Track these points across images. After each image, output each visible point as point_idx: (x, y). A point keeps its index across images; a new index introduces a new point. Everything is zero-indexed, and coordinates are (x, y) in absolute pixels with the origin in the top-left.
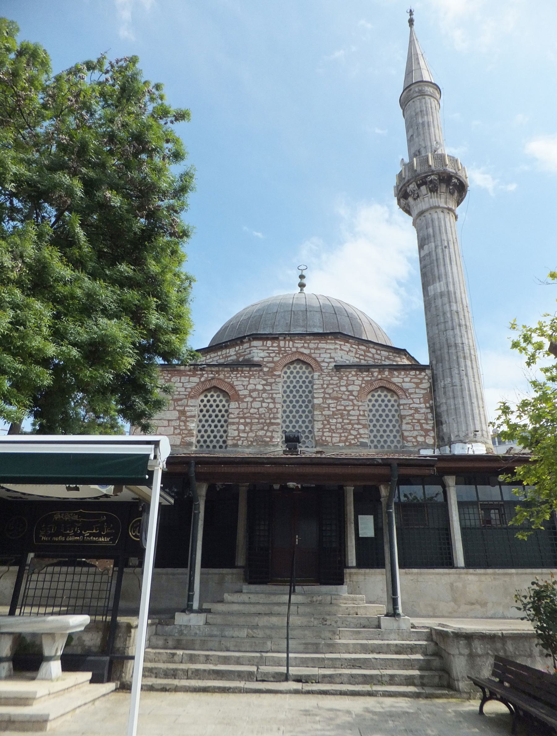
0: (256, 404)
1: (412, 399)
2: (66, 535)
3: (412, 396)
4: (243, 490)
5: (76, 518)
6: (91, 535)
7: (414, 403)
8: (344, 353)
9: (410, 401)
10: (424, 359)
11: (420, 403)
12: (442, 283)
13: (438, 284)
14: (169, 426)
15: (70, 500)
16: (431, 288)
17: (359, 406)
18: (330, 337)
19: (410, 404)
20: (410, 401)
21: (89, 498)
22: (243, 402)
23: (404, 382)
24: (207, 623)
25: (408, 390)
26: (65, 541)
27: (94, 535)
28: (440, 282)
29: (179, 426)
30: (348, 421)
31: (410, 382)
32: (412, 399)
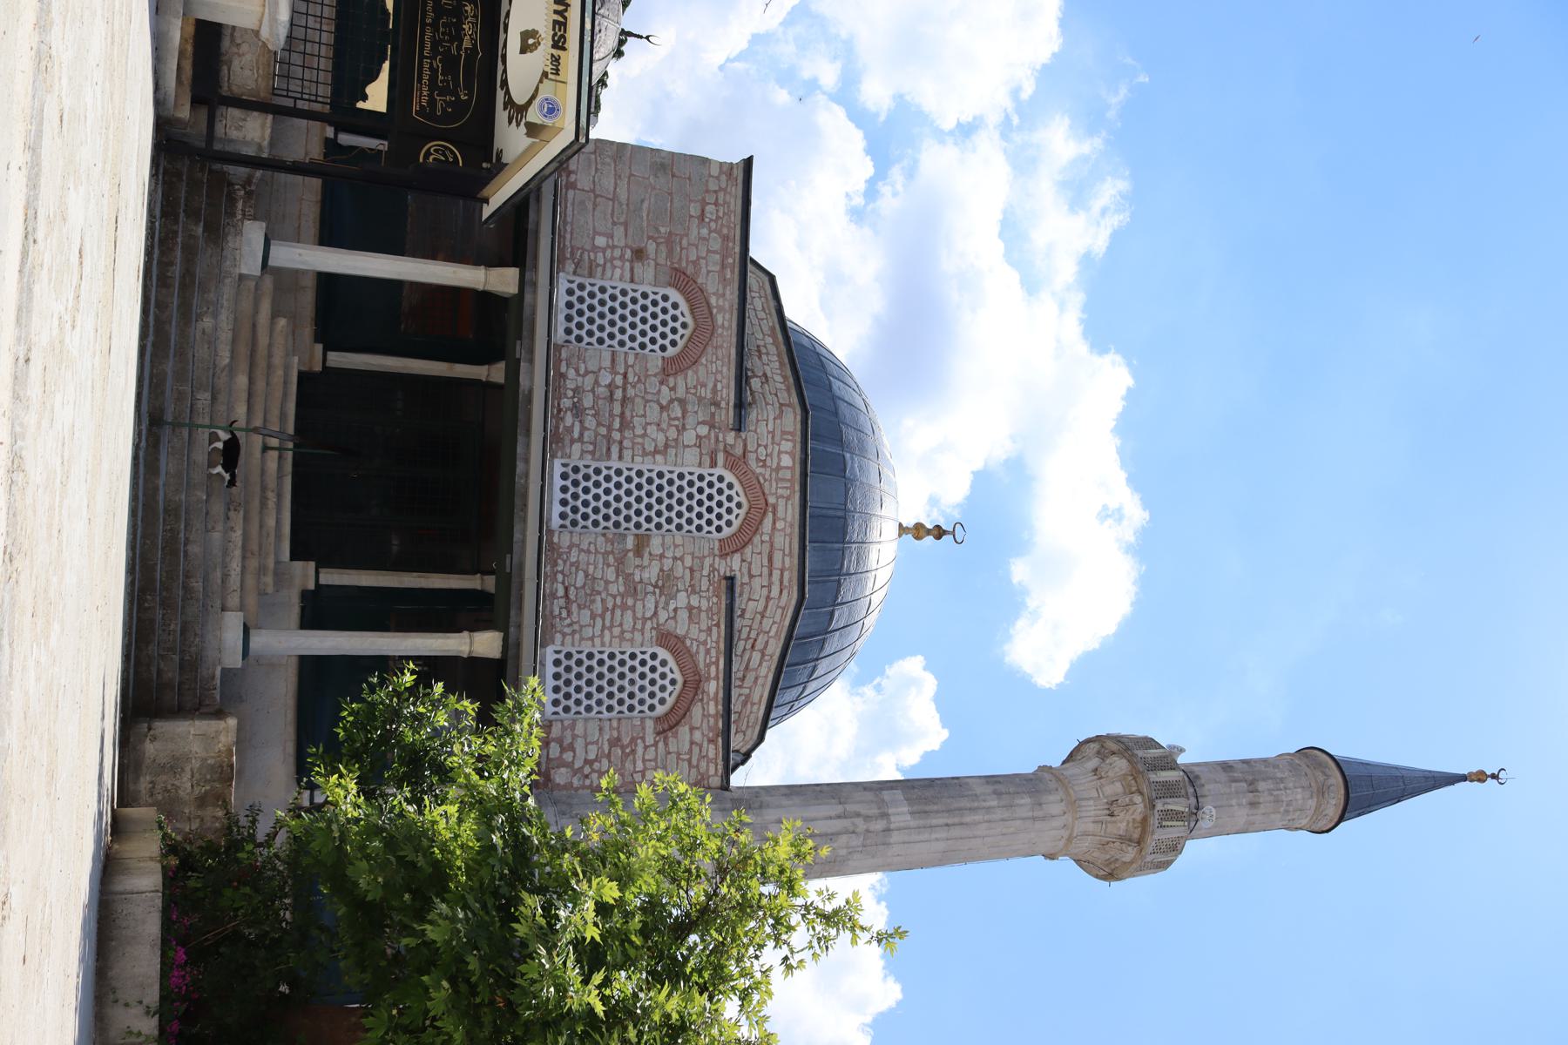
0: (653, 412)
1: (656, 744)
2: (435, 26)
3: (661, 745)
4: (496, 373)
5: (467, 43)
6: (433, 70)
7: (646, 747)
8: (768, 608)
9: (650, 740)
10: (738, 779)
11: (644, 761)
12: (909, 817)
13: (905, 809)
14: (614, 223)
15: (502, 36)
16: (899, 794)
17: (642, 631)
18: (132, 787)
19: (643, 739)
20: (650, 740)
21: (505, 71)
22: (661, 383)
23: (692, 729)
24: (242, 277)
25: (675, 736)
26: (424, 25)
27: (433, 79)
28: (911, 813)
29: (614, 247)
30: (610, 605)
31: (692, 743)
32: (656, 744)
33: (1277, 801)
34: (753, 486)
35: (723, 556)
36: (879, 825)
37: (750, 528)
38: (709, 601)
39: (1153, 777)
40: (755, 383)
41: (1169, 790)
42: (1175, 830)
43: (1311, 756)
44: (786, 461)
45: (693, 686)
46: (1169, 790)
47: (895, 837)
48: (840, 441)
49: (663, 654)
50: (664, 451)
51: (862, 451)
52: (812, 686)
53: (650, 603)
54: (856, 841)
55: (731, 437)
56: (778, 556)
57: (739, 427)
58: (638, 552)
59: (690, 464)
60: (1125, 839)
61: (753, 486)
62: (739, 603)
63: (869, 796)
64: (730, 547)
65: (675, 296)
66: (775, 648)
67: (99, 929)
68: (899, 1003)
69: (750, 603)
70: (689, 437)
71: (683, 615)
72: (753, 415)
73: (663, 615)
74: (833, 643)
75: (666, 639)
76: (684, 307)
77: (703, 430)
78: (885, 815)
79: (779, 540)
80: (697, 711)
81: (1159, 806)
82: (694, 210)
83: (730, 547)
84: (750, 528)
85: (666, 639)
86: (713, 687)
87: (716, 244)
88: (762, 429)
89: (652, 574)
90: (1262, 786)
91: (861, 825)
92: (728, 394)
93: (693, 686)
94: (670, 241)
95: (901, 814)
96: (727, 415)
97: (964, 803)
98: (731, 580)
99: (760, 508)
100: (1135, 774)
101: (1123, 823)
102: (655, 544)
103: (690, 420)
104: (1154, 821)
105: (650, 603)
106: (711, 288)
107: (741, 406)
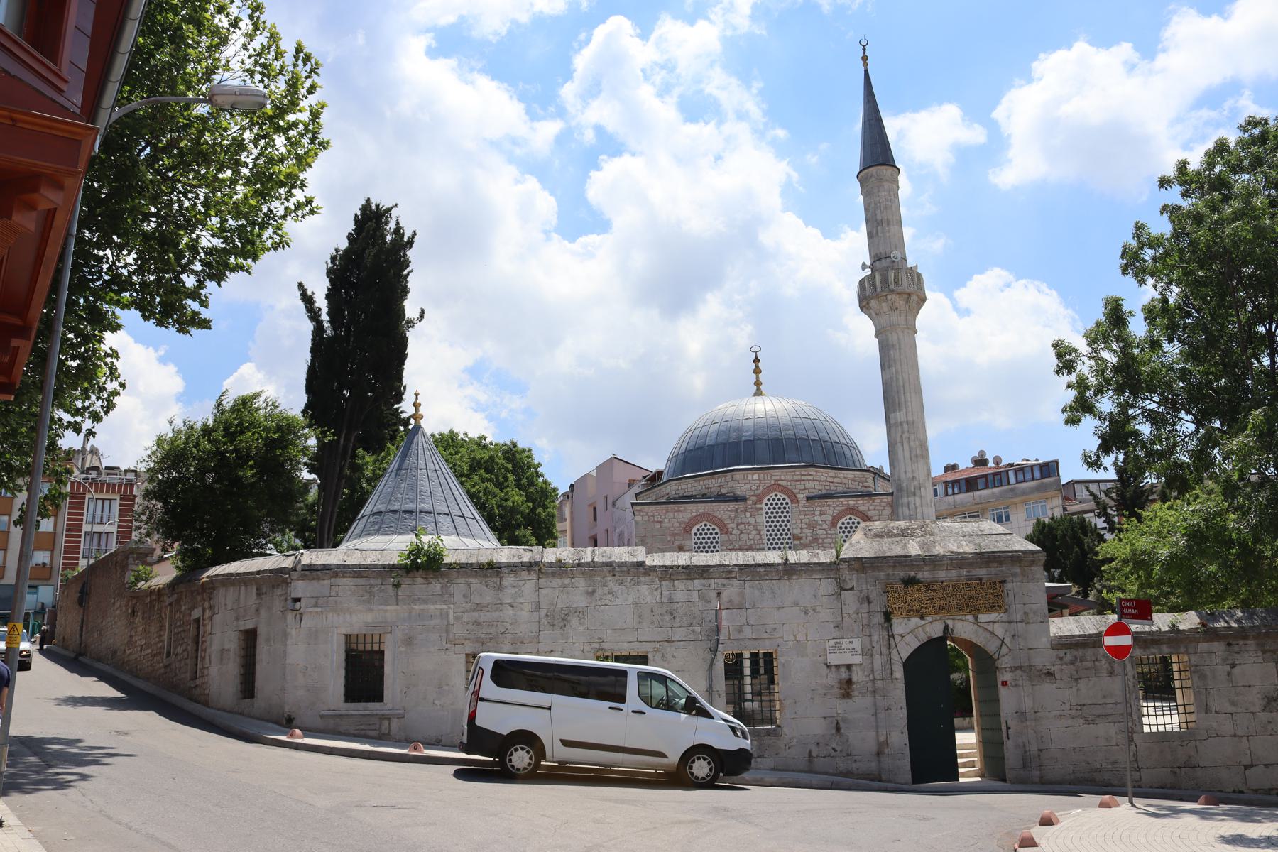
0: (744, 537)
33: (886, 208)
34: (768, 490)
35: (798, 502)
36: (905, 426)
37: (785, 490)
38: (817, 506)
39: (879, 289)
40: (724, 491)
41: (885, 282)
42: (903, 277)
43: (863, 178)
44: (756, 477)
45: (851, 510)
46: (885, 282)
47: (910, 419)
48: (737, 443)
49: (840, 524)
50: (759, 531)
51: (739, 430)
52: (843, 441)
53: (820, 532)
54: (912, 437)
55: (749, 502)
56: (796, 478)
57: (744, 499)
58: (800, 538)
59: (762, 519)
60: (908, 301)
61: (768, 490)
62: (816, 493)
63: (893, 430)
64: (795, 500)
65: (694, 531)
66: (832, 473)
67: (255, 647)
68: (1035, 58)
69: (817, 488)
70: (752, 520)
71: (824, 517)
72: (739, 493)
73: (825, 526)
74: (824, 435)
75: (834, 524)
76: (698, 526)
77: (748, 514)
78: (901, 423)
79: (789, 478)
80: (862, 509)
81: (892, 287)
82: (658, 526)
83: (795, 500)
84: (785, 490)
85: (834, 524)
86: (852, 502)
87: (670, 515)
88: (744, 488)
89: (808, 532)
90: (879, 217)
91: (905, 435)
92: (732, 505)
93: (851, 510)
94: (673, 535)
95: (900, 416)
96: (741, 505)
97: (894, 384)
98: (808, 498)
99: (777, 487)
100: (878, 297)
101: (900, 303)
102: (797, 531)
103: (745, 520)
104: (899, 289)
105: (820, 532)
106: (689, 516)
107: (736, 499)
